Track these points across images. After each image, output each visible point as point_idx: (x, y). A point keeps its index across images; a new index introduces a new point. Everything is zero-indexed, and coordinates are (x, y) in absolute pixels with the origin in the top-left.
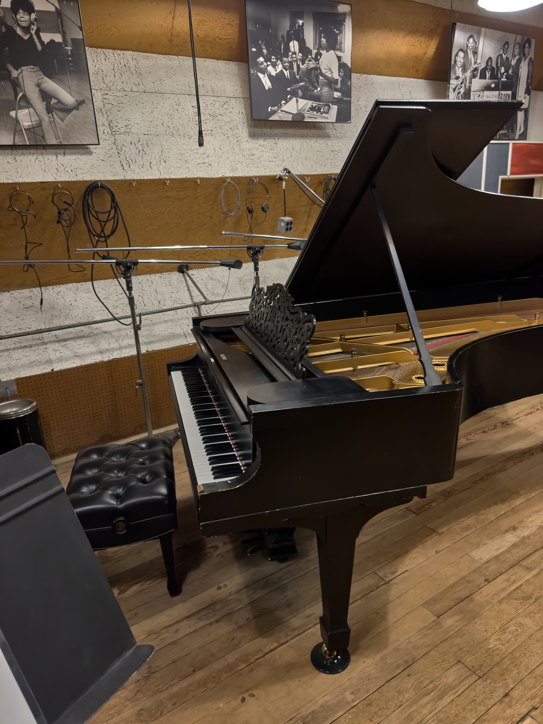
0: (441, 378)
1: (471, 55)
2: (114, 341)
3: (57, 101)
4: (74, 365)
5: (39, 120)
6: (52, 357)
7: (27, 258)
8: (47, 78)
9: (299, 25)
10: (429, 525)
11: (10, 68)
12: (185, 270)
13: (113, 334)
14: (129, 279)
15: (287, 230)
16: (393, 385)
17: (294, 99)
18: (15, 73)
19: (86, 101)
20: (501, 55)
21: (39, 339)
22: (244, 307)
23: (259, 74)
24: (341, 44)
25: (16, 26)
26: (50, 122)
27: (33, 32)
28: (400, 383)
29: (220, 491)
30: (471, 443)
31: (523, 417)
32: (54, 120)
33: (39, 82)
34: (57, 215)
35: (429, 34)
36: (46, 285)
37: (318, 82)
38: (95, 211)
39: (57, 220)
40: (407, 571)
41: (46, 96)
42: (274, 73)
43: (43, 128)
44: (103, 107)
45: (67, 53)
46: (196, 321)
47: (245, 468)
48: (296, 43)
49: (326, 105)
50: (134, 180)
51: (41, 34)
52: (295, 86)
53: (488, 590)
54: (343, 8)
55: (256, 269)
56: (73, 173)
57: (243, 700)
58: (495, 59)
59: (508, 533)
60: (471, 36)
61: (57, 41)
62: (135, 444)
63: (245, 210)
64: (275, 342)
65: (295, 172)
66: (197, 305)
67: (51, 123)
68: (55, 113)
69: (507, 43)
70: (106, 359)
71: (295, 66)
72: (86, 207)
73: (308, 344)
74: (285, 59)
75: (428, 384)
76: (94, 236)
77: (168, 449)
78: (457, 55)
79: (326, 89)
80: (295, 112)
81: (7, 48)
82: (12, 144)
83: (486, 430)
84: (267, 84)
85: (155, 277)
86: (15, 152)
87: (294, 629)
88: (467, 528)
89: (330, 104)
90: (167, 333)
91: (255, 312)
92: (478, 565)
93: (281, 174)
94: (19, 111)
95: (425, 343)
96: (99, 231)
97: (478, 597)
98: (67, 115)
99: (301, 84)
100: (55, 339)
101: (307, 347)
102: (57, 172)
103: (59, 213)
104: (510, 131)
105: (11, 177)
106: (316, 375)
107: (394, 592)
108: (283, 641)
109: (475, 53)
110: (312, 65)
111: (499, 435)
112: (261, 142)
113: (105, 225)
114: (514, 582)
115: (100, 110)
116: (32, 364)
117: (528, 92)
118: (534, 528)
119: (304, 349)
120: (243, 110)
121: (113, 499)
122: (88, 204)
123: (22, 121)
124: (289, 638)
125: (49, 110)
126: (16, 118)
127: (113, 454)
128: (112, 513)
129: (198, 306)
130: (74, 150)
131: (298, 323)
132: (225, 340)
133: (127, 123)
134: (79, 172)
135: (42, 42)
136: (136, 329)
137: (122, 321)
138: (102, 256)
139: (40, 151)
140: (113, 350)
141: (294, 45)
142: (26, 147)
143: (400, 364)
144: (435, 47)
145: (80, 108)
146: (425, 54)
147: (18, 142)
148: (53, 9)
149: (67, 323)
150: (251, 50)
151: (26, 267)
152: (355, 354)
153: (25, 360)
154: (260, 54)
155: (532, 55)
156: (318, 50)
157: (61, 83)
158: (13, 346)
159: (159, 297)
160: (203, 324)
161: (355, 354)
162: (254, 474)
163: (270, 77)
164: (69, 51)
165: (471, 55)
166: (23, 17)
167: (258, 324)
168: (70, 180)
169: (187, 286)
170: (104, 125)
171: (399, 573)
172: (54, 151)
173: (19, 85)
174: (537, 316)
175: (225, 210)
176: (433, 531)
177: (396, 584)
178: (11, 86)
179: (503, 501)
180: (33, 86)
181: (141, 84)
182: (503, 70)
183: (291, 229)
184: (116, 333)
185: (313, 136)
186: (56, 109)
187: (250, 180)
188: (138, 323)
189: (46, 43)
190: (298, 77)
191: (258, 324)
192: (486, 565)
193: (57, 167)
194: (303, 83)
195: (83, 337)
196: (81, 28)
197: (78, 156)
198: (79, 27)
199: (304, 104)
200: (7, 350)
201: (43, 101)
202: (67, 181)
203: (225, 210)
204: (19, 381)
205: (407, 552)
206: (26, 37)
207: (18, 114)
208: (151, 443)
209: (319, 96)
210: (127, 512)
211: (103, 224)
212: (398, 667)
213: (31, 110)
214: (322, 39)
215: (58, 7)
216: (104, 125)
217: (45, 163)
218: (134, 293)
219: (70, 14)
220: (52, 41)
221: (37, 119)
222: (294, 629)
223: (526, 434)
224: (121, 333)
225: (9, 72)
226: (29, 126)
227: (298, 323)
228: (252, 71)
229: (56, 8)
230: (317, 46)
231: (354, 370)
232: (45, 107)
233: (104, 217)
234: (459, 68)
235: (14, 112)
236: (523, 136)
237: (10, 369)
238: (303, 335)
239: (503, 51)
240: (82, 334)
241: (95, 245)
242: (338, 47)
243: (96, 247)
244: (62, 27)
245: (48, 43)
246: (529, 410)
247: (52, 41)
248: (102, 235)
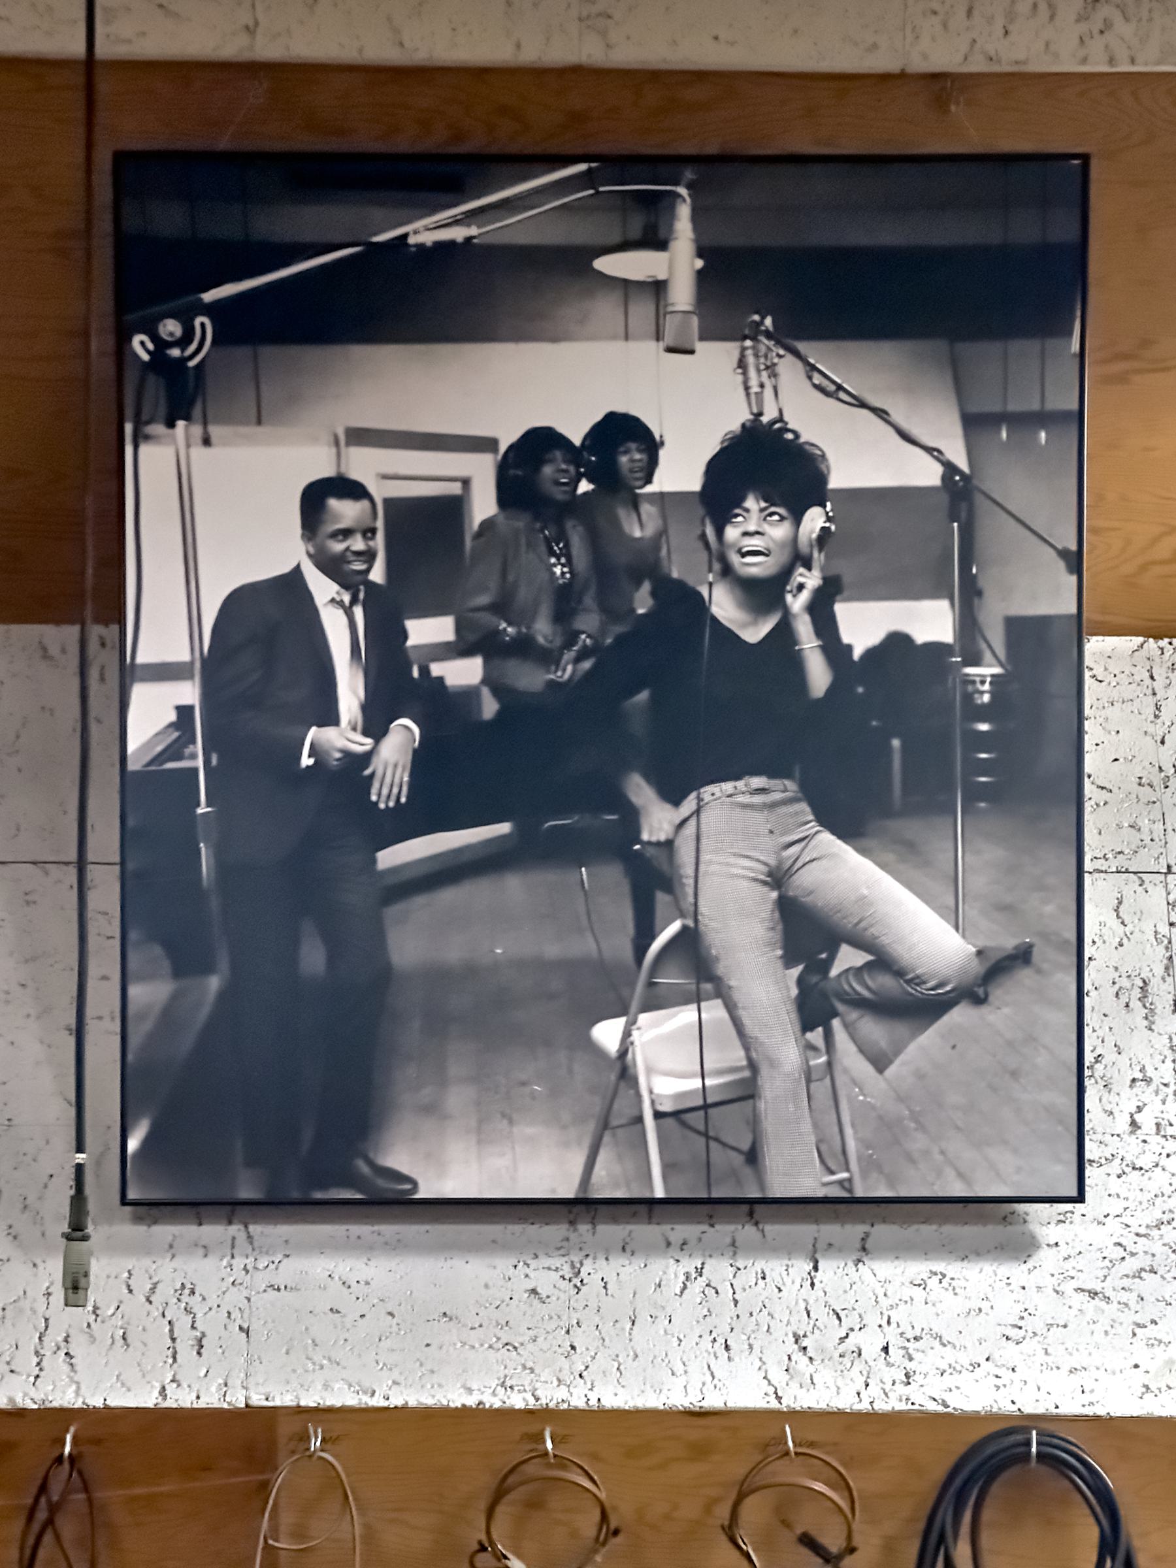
3: (870, 958)
5: (744, 1063)
8: (833, 838)
25: (711, 577)
26: (809, 1075)
27: (797, 603)
32: (829, 1064)
33: (780, 862)
43: (761, 1105)
44: (1159, 970)
45: (968, 698)
51: (842, 610)
56: (889, 1365)
61: (921, 636)
67: (809, 1081)
68: (846, 1026)
81: (643, 696)
86: (588, 1237)
94: (643, 1018)
98: (914, 1035)
102: (798, 1356)
105: (527, 1378)
115: (1136, 993)
123: (650, 1071)
126: (623, 1053)
130: (928, 1230)
139: (724, 1231)
142: (650, 1211)
145: (997, 993)
148: (929, 475)
164: (987, 687)
168: (864, 1406)
170: (1148, 1081)
172: (806, 1231)
173: (669, 883)
178: (625, 887)
180: (745, 884)
186: (860, 1003)
189: (857, 654)
193: (804, 1327)
196: (1074, 561)
197: (939, 1266)
198: (1063, 554)
201: (789, 960)
202: (840, 1413)
206: (755, 633)
207: (635, 1034)
213: (714, 1011)
216: (1148, 1081)
217: (736, 1302)
220: (897, 642)
221: (737, 1056)
225: (631, 817)
232: (794, 992)
235: (619, 1023)
244: (967, 559)
245: (870, 654)
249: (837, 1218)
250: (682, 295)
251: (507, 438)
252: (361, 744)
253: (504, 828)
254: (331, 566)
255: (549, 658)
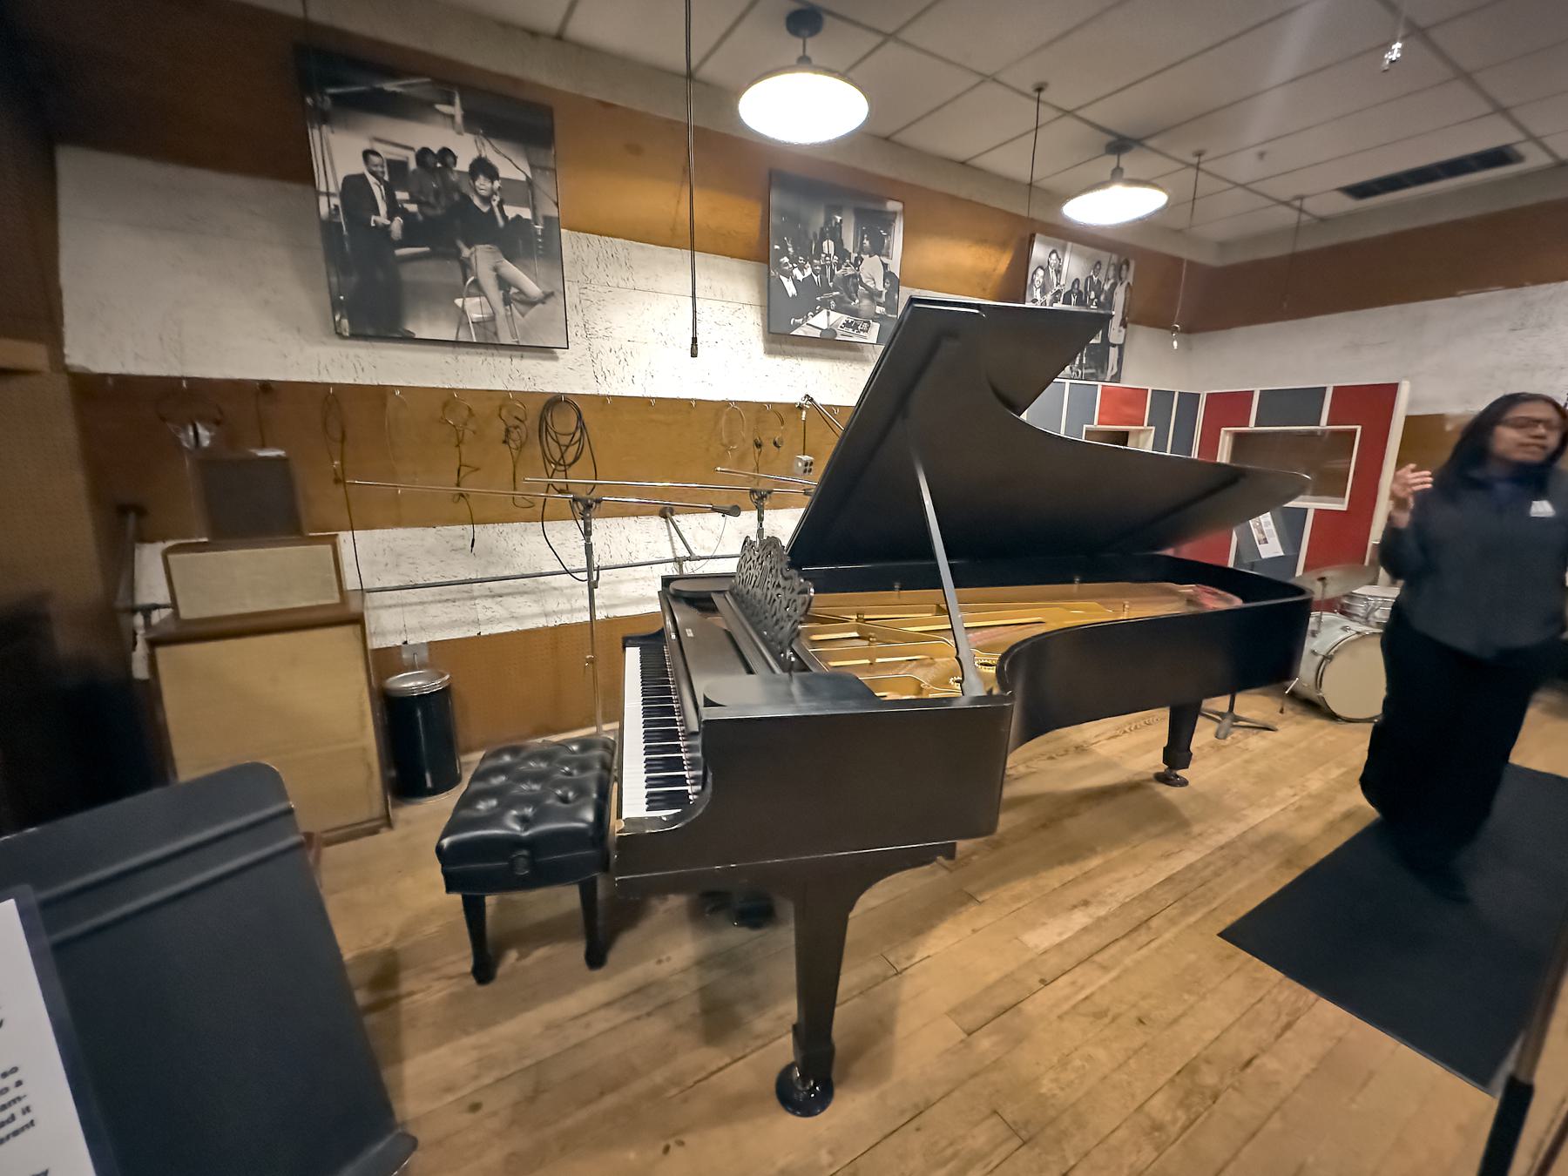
0: (985, 684)
1: (1053, 275)
2: (565, 601)
4: (508, 630)
6: (481, 617)
7: (458, 485)
9: (836, 222)
10: (965, 889)
11: (461, 245)
12: (669, 514)
13: (565, 591)
14: (589, 521)
15: (805, 471)
16: (920, 690)
17: (825, 311)
18: (466, 252)
19: (556, 293)
20: (1091, 277)
21: (467, 592)
22: (730, 566)
23: (781, 277)
24: (888, 248)
26: (506, 316)
27: (495, 204)
28: (931, 687)
29: (647, 831)
30: (1034, 773)
31: (1105, 742)
34: (504, 433)
35: (1003, 245)
36: (484, 522)
37: (856, 292)
38: (555, 432)
39: (503, 438)
40: (929, 957)
41: (504, 283)
42: (800, 277)
45: (536, 232)
46: (667, 581)
47: (695, 797)
48: (831, 243)
49: (864, 322)
50: (609, 396)
51: (505, 207)
52: (826, 295)
53: (1045, 997)
54: (893, 206)
55: (760, 519)
57: (667, 1149)
58: (1084, 281)
59: (1076, 910)
60: (1054, 252)
62: (564, 745)
63: (752, 442)
64: (762, 617)
65: (820, 400)
66: (678, 561)
69: (1099, 263)
70: (552, 624)
71: (828, 271)
72: (543, 426)
73: (801, 623)
74: (815, 261)
75: (966, 693)
76: (550, 462)
77: (608, 756)
78: (1035, 272)
79: (866, 302)
80: (825, 327)
82: (454, 339)
83: (1054, 755)
84: (791, 290)
85: (629, 522)
87: (758, 1037)
88: (1018, 898)
89: (871, 321)
90: (636, 594)
91: (742, 574)
92: (1028, 956)
93: (802, 402)
94: (467, 299)
95: (967, 633)
96: (557, 456)
97: (1028, 1007)
99: (835, 293)
100: (488, 593)
101: (800, 627)
103: (507, 431)
104: (1099, 371)
106: (811, 667)
107: (908, 988)
108: (739, 1055)
109: (1058, 272)
110: (850, 270)
111: (1071, 763)
112: (778, 360)
113: (566, 450)
114: (1083, 988)
116: (454, 624)
117: (1124, 324)
118: (1115, 905)
119: (795, 629)
120: (759, 321)
121: (516, 822)
122: (547, 423)
124: (748, 1050)
125: (507, 301)
127: (532, 757)
128: (514, 843)
129: (679, 562)
131: (791, 592)
132: (702, 609)
133: (608, 325)
134: (538, 381)
135: (505, 217)
136: (592, 586)
137: (577, 575)
138: (558, 489)
139: (490, 351)
140: (562, 612)
141: (829, 246)
143: (936, 660)
144: (1008, 262)
146: (994, 270)
147: (463, 337)
148: (523, 178)
149: (506, 573)
150: (773, 247)
151: (457, 497)
152: (872, 642)
153: (444, 618)
154: (785, 252)
155: (1130, 280)
156: (859, 254)
157: (524, 268)
158: (431, 599)
159: (631, 547)
160: (674, 586)
161: (872, 642)
162: (700, 811)
163: (795, 281)
165: (1053, 275)
166: (483, 184)
167: (745, 591)
169: (670, 534)
171: (917, 959)
172: (509, 353)
173: (471, 268)
174: (1127, 606)
175: (725, 441)
176: (971, 898)
177: (911, 975)
179: (1072, 860)
181: (631, 279)
182: (1093, 295)
183: (810, 470)
184: (568, 591)
185: (846, 359)
186: (516, 300)
187: (761, 407)
188: (595, 579)
190: (831, 284)
191: (745, 591)
192: (1044, 957)
194: (838, 293)
195: (526, 593)
196: (557, 204)
199: (837, 318)
200: (422, 603)
201: (500, 289)
203: (725, 441)
204: (431, 645)
205: (932, 927)
208: (586, 744)
209: (857, 310)
210: (531, 844)
211: (563, 448)
212: (902, 1112)
213: (484, 299)
214: (865, 241)
215: (530, 175)
218: (593, 539)
219: (545, 185)
222: (758, 1037)
223: (1108, 765)
224: (574, 591)
225: (459, 251)
226: (479, 318)
227: (791, 592)
228: (773, 273)
229: (527, 177)
230: (858, 250)
231: (871, 664)
233: (565, 440)
234: (1037, 289)
236: (1116, 378)
237: (422, 629)
238: (795, 610)
239: (1094, 272)
240: (525, 589)
241: (550, 475)
242: (884, 251)
243: (551, 478)
246: (1113, 733)
247: (518, 217)
248: (562, 462)
249: (516, 350)
250: (459, 119)
251: (418, 147)
252: (388, 222)
253: (679, 810)
254: (373, 174)
255: (433, 207)
